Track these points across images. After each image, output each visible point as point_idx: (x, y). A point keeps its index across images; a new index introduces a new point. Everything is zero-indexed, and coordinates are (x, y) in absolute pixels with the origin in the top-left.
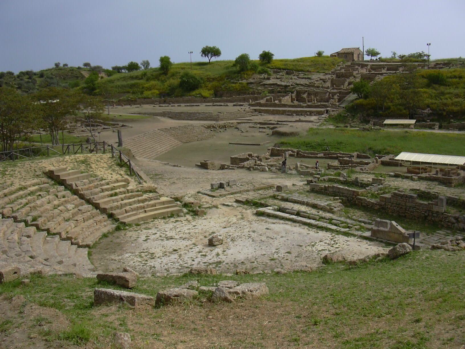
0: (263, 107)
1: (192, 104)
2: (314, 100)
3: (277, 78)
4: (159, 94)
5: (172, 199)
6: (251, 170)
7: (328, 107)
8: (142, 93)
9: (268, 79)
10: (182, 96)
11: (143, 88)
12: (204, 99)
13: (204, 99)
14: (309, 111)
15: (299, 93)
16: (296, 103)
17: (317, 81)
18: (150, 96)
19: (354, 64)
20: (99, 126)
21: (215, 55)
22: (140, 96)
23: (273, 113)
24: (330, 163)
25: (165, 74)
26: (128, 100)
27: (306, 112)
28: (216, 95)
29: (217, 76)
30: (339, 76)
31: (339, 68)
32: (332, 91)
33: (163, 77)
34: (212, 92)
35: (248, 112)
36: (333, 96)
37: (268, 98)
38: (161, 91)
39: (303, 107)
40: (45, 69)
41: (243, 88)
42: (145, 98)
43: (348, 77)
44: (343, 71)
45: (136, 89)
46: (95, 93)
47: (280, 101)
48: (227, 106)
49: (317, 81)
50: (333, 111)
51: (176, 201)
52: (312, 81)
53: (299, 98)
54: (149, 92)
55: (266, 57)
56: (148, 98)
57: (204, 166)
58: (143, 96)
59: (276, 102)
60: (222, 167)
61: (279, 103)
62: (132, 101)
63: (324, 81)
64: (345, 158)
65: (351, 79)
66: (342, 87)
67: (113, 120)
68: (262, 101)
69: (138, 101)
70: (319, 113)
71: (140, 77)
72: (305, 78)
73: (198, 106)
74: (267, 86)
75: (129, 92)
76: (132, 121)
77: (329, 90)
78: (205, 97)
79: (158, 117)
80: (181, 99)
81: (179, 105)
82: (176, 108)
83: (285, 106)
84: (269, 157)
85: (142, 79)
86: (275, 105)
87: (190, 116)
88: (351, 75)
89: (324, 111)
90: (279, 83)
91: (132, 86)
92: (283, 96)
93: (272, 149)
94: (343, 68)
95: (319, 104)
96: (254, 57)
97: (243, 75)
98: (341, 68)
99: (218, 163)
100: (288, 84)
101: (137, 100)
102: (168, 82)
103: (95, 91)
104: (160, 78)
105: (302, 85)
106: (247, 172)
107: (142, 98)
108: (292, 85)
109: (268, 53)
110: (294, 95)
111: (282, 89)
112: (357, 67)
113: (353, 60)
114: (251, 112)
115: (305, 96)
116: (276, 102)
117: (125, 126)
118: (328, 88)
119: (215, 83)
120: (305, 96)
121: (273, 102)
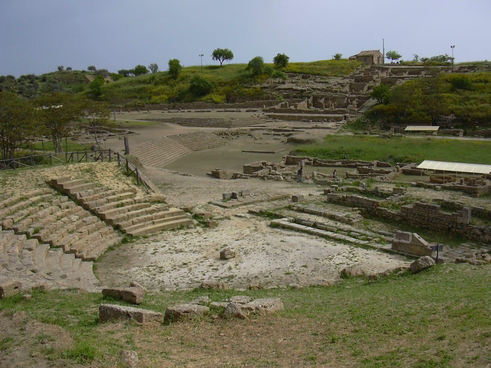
0: (278, 113)
1: (203, 110)
2: (332, 106)
3: (293, 83)
4: (168, 99)
5: (181, 210)
6: (265, 180)
7: (346, 113)
8: (150, 98)
9: (284, 83)
10: (192, 101)
11: (151, 92)
12: (215, 105)
13: (216, 105)
14: (326, 117)
15: (315, 98)
16: (312, 108)
17: (335, 85)
18: (159, 101)
19: (373, 68)
20: (104, 132)
21: (227, 58)
22: (148, 101)
23: (288, 119)
24: (348, 172)
25: (175, 78)
26: (135, 106)
27: (323, 118)
28: (228, 100)
29: (229, 80)
30: (358, 80)
31: (358, 72)
32: (351, 96)
33: (172, 82)
34: (224, 97)
35: (262, 118)
36: (351, 101)
37: (283, 103)
38: (170, 96)
39: (320, 113)
40: (47, 72)
41: (257, 93)
42: (153, 104)
43: (367, 82)
44: (362, 74)
45: (144, 94)
46: (100, 98)
47: (296, 106)
48: (240, 111)
49: (335, 85)
50: (352, 117)
51: (186, 212)
52: (330, 85)
53: (316, 103)
54: (158, 97)
55: (281, 60)
56: (157, 103)
57: (215, 175)
58: (151, 101)
59: (292, 107)
60: (235, 177)
61: (294, 109)
62: (140, 106)
63: (342, 85)
64: (365, 167)
65: (371, 83)
66: (361, 92)
67: (119, 126)
68: (277, 107)
69: (146, 106)
70: (337, 120)
71: (148, 81)
72: (322, 82)
73: (210, 111)
74: (282, 91)
75: (136, 97)
76: (140, 127)
77: (347, 95)
78: (216, 103)
79: (167, 124)
80: (191, 104)
81: (188, 110)
82: (186, 114)
83: (301, 111)
84: (284, 166)
85: (150, 83)
86: (291, 111)
87: (200, 123)
88: (371, 79)
89: (342, 117)
90: (295, 87)
91: (140, 91)
92: (299, 102)
93: (287, 157)
94: (362, 72)
95: (337, 109)
96: (269, 60)
97: (256, 79)
98: (360, 72)
99: (230, 172)
100: (304, 89)
101: (145, 105)
102: (177, 86)
103: (100, 96)
104: (169, 82)
105: (319, 90)
106: (261, 181)
107: (150, 103)
108: (308, 90)
109: (283, 56)
110: (310, 100)
111: (298, 93)
112: (377, 70)
113: (373, 63)
114: (265, 118)
115: (322, 101)
116: (292, 107)
117: (132, 133)
118: (346, 93)
119: (227, 88)
120: (322, 101)
121: (288, 108)
